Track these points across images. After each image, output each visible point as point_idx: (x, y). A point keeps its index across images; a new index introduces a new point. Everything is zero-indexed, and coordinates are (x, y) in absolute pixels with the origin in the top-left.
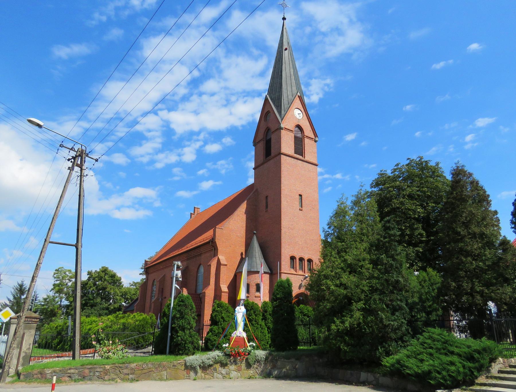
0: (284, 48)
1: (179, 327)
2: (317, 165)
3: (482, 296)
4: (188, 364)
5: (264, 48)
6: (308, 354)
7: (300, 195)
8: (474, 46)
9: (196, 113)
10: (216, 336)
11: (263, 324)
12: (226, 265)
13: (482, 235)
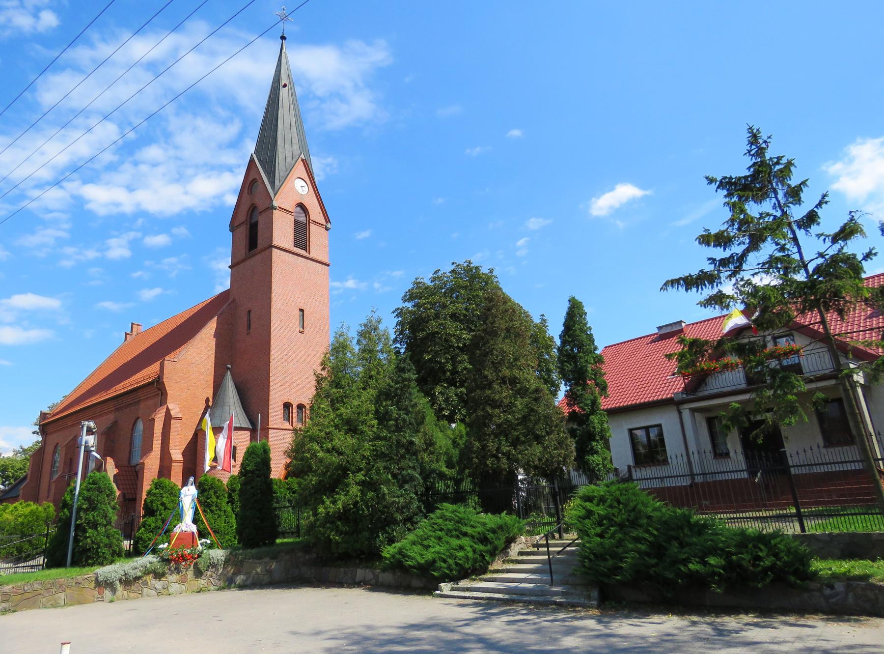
0: (282, 83)
1: (88, 524)
2: (328, 265)
3: (508, 459)
4: (101, 579)
5: (234, 109)
6: (290, 549)
7: (302, 310)
8: (516, 133)
9: (130, 189)
10: (152, 532)
11: (229, 509)
12: (180, 419)
13: (513, 381)
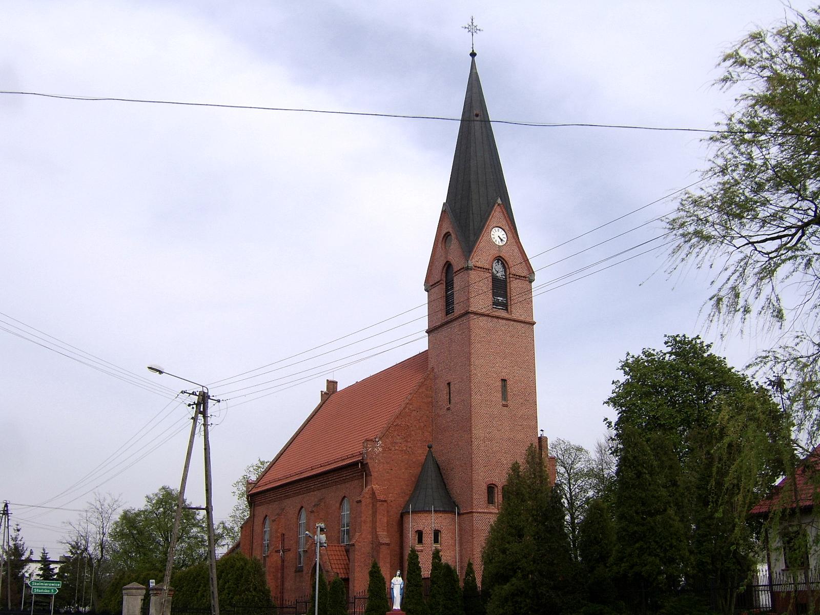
7: (504, 381)
